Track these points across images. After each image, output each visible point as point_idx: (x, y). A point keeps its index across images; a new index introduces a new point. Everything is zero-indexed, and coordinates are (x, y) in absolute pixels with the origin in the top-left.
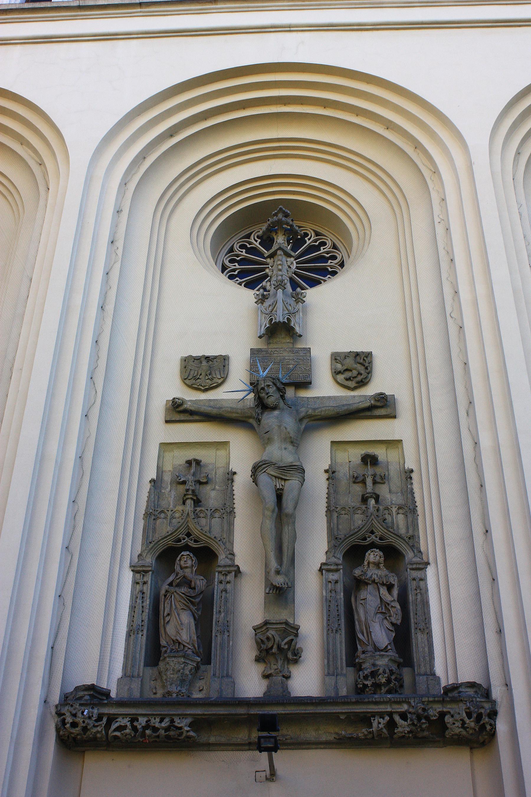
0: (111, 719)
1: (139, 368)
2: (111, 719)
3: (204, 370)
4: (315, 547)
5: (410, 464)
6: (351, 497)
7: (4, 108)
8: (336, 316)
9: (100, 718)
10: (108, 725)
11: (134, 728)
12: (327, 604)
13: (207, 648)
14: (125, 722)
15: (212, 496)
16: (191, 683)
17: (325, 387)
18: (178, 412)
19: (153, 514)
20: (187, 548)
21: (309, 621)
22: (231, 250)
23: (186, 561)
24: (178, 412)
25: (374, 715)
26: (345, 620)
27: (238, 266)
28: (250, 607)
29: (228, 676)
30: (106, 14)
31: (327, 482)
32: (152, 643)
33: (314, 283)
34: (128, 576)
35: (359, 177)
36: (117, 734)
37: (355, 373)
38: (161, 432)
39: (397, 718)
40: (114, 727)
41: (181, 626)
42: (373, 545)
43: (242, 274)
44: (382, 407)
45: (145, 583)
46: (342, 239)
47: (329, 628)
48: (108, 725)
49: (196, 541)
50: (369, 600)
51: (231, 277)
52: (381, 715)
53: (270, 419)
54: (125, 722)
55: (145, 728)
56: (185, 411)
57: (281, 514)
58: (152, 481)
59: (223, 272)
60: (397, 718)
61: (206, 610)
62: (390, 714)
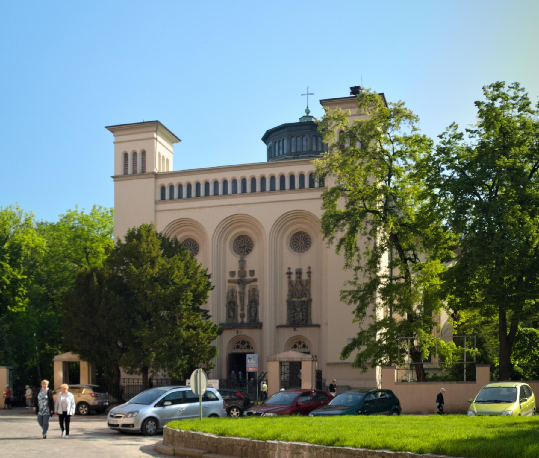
3: (232, 274)
4: (247, 302)
7: (368, 414)
8: (252, 261)
12: (248, 310)
13: (235, 316)
15: (234, 294)
17: (248, 277)
18: (230, 281)
19: (228, 297)
21: (246, 312)
23: (232, 304)
26: (249, 312)
28: (239, 312)
29: (237, 320)
32: (229, 316)
33: (196, 254)
38: (228, 285)
41: (232, 314)
44: (255, 280)
46: (160, 396)
47: (248, 313)
50: (253, 309)
57: (242, 300)
61: (234, 311)
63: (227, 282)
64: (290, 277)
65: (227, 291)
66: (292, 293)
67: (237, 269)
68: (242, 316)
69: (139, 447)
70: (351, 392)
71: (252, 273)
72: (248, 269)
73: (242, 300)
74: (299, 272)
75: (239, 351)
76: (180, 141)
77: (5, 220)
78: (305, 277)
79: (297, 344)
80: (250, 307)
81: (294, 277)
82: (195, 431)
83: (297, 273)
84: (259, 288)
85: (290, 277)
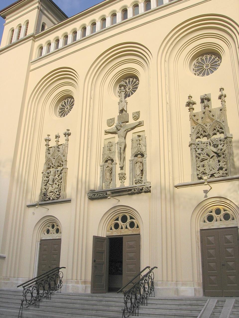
0: (95, 195)
1: (39, 141)
5: (146, 136)
6: (135, 145)
8: (133, 104)
10: (94, 196)
14: (97, 195)
16: (109, 185)
17: (132, 121)
20: (109, 160)
22: (194, 69)
24: (107, 132)
25: (132, 189)
27: (198, 72)
30: (125, 24)
34: (99, 167)
36: (96, 197)
40: (95, 196)
42: (139, 154)
44: (140, 124)
45: (102, 168)
48: (94, 196)
51: (198, 75)
52: (133, 189)
53: (119, 132)
54: (97, 195)
56: (107, 132)
58: (103, 148)
59: (196, 75)
62: (135, 189)
63: (103, 133)
64: (191, 109)
65: (103, 146)
66: (200, 133)
68: (122, 177)
70: (234, 313)
71: (136, 116)
72: (130, 111)
74: (205, 100)
75: (115, 233)
76: (145, 130)
78: (215, 104)
79: (214, 214)
80: (134, 163)
81: (198, 108)
83: (202, 101)
84: (146, 134)
85: (191, 109)
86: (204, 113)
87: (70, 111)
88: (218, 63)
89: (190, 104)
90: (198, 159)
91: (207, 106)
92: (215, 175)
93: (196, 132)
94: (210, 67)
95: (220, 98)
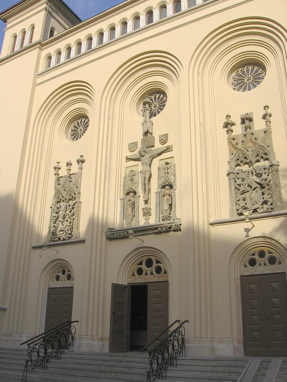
0: (114, 234)
2: (114, 234)
5: (175, 163)
6: (162, 174)
8: (160, 125)
9: (112, 234)
10: (113, 235)
11: (118, 235)
14: (116, 234)
16: (131, 223)
17: (158, 146)
20: (131, 192)
22: (232, 83)
24: (128, 159)
25: (159, 227)
27: (237, 87)
28: (141, 205)
31: (264, 121)
34: (119, 201)
35: (173, 73)
36: (115, 237)
37: (164, 140)
39: (163, 227)
40: (114, 235)
42: (167, 185)
43: (240, 88)
44: (168, 149)
45: (122, 202)
49: (133, 190)
53: (143, 159)
54: (116, 234)
55: (119, 235)
56: (129, 159)
58: (124, 177)
60: (163, 227)
62: (162, 227)
63: (124, 159)
64: (230, 131)
65: (123, 175)
66: (241, 159)
67: (139, 137)
68: (147, 213)
69: (258, 266)
71: (164, 139)
72: (157, 133)
73: (147, 191)
74: (247, 120)
77: (171, 365)
78: (259, 125)
80: (161, 196)
81: (238, 130)
82: (163, 339)
83: (243, 122)
84: (176, 161)
85: (230, 131)
86: (245, 136)
87: (84, 133)
88: (261, 76)
89: (228, 125)
90: (238, 191)
91: (249, 127)
92: (258, 210)
93: (236, 158)
94: (252, 81)
95: (264, 117)
